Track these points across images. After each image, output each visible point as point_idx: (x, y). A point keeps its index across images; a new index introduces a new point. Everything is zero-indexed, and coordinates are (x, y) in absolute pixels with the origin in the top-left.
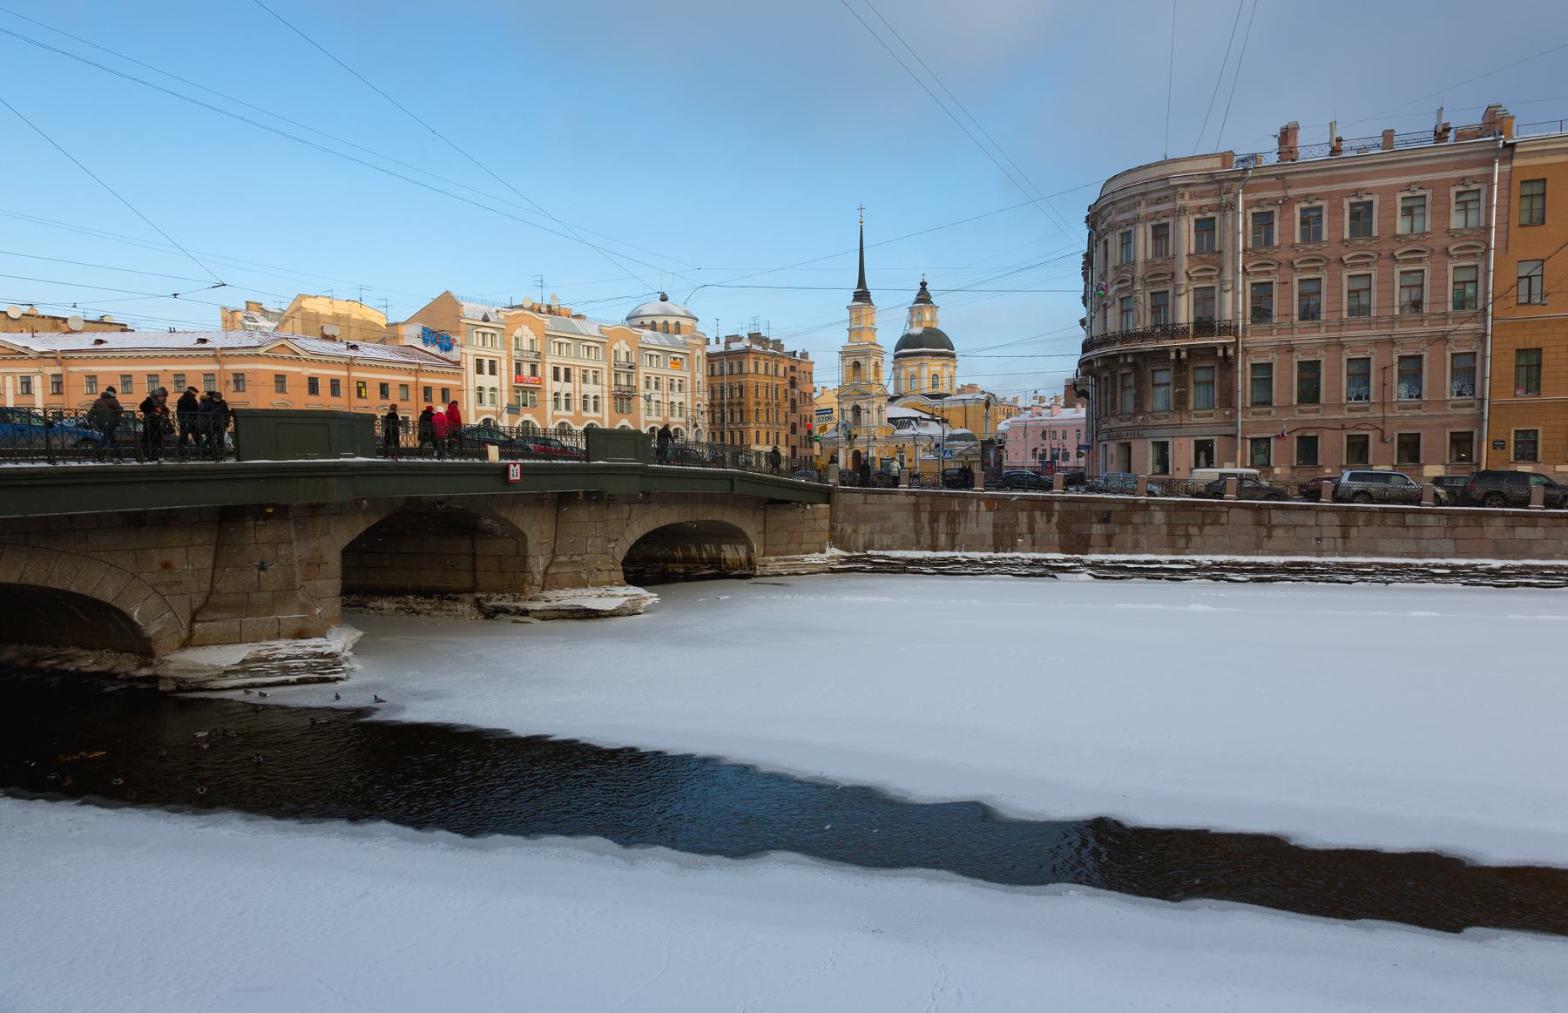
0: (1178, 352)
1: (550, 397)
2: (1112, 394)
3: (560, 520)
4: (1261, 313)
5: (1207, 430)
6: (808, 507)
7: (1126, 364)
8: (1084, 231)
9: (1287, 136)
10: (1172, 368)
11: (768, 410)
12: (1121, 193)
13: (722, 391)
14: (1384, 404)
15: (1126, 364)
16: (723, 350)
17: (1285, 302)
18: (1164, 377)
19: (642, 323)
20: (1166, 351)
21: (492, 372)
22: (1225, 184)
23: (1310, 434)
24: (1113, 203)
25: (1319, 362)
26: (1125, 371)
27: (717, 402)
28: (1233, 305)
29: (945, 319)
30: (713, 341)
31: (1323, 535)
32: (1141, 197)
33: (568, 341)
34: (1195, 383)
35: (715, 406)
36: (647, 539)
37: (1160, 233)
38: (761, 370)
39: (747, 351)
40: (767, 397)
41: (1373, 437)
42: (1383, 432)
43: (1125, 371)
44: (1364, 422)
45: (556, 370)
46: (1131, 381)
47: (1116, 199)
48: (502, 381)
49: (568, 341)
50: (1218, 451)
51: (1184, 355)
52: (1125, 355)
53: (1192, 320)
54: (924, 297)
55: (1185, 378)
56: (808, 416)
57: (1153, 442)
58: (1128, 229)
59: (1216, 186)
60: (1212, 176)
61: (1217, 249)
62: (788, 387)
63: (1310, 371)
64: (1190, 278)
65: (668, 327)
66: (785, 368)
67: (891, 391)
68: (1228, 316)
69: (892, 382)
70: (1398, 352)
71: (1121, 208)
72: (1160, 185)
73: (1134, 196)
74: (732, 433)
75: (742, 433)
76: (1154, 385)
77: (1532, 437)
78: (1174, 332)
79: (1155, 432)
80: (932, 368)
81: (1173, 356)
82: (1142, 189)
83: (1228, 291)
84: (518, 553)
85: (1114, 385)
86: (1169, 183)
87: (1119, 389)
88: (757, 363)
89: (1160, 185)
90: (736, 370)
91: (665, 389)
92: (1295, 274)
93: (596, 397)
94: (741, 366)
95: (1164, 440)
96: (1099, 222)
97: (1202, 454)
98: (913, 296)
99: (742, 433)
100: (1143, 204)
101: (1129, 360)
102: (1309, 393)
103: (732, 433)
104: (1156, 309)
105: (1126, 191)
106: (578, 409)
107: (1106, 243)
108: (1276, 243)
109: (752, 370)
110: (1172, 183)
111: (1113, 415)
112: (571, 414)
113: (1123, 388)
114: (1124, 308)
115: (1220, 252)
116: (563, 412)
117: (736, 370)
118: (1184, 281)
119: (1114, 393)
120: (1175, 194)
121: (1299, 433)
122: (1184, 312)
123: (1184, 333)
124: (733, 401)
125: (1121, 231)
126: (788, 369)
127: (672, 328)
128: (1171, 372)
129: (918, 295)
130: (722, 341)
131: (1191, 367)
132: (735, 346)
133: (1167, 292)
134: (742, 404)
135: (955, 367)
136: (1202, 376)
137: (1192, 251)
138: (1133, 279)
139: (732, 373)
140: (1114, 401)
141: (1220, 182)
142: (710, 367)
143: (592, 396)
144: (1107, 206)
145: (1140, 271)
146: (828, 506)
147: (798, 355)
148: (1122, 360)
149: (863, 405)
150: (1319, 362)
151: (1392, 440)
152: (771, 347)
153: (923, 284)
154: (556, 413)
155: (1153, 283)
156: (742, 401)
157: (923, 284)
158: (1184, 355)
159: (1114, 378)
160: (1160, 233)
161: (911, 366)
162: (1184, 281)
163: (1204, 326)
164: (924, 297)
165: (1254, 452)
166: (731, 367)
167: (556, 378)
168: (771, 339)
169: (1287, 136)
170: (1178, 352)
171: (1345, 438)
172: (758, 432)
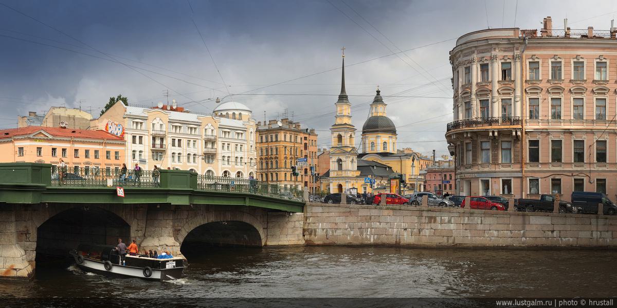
0: (493, 132)
1: (130, 153)
2: (462, 154)
3: (148, 222)
4: (534, 115)
5: (508, 175)
6: (291, 214)
7: (467, 138)
8: (450, 67)
9: (547, 22)
10: (491, 141)
11: (291, 161)
12: (465, 45)
13: (272, 150)
14: (590, 164)
15: (467, 138)
16: (267, 128)
17: (545, 110)
18: (487, 145)
19: (221, 114)
20: (487, 131)
21: (141, 143)
22: (516, 45)
23: (557, 177)
24: (461, 51)
25: (561, 141)
26: (468, 141)
27: (264, 157)
28: (519, 110)
29: (391, 112)
30: (262, 124)
31: (555, 229)
32: (519, 45)
33: (180, 125)
34: (502, 149)
35: (273, 158)
36: (190, 234)
37: (484, 68)
38: (288, 139)
39: (280, 129)
40: (291, 154)
41: (586, 180)
42: (590, 178)
43: (468, 141)
44: (581, 172)
45: (134, 137)
46: (470, 147)
47: (462, 49)
48: (146, 147)
49: (180, 125)
50: (180, 187)
51: (496, 134)
52: (467, 133)
53: (501, 116)
54: (378, 100)
55: (497, 147)
56: (239, 164)
57: (482, 180)
58: (468, 65)
59: (512, 46)
60: (509, 39)
61: (512, 79)
62: (303, 149)
63: (557, 145)
64: (499, 94)
65: (235, 116)
66: (301, 138)
67: (360, 152)
68: (519, 114)
69: (361, 146)
70: (551, 138)
71: (465, 53)
72: (483, 43)
73: (471, 48)
74: (272, 174)
75: (277, 174)
76: (482, 150)
77: (581, 182)
78: (491, 122)
79: (483, 175)
80: (371, 139)
81: (491, 134)
82: (475, 44)
83: (518, 101)
84: (560, 232)
85: (463, 149)
86: (488, 42)
87: (465, 150)
88: (296, 137)
89: (483, 43)
90: (274, 140)
91: (185, 146)
92: (549, 95)
93: (179, 154)
94: (276, 137)
95: (487, 179)
96: (455, 61)
97: (506, 187)
98: (373, 99)
99: (277, 174)
100: (476, 52)
101: (469, 135)
102: (557, 156)
103: (272, 174)
104: (504, 109)
105: (468, 44)
106: (185, 161)
107: (458, 72)
108: (563, 78)
109: (283, 139)
110: (489, 42)
111: (462, 165)
112: (230, 166)
113: (467, 151)
114: (467, 108)
115: (514, 81)
116: (227, 166)
117: (274, 140)
118: (496, 94)
119: (463, 153)
120: (491, 49)
121: (552, 177)
122: (497, 112)
123: (476, 123)
124: (272, 156)
125: (465, 66)
126: (303, 139)
127: (237, 116)
128: (490, 143)
129: (376, 98)
130: (268, 123)
131: (500, 141)
132: (274, 126)
133: (488, 100)
134: (277, 158)
135: (396, 138)
136: (505, 145)
137: (501, 79)
138: (471, 92)
139: (272, 141)
140: (463, 157)
141: (513, 44)
142: (260, 138)
143: (192, 154)
144: (458, 52)
145: (474, 89)
146: (303, 214)
147: (309, 131)
148: (465, 136)
149: (343, 158)
150: (561, 141)
151: (594, 182)
152: (294, 126)
153: (378, 92)
154: (223, 166)
155: (481, 95)
156: (277, 156)
157: (378, 92)
158: (496, 134)
159: (462, 145)
160: (484, 68)
161: (371, 138)
162: (496, 94)
163: (507, 119)
164: (378, 100)
165: (531, 186)
166: (272, 138)
167: (134, 142)
168: (294, 122)
169: (547, 22)
170: (493, 132)
171: (573, 180)
172: (286, 174)
